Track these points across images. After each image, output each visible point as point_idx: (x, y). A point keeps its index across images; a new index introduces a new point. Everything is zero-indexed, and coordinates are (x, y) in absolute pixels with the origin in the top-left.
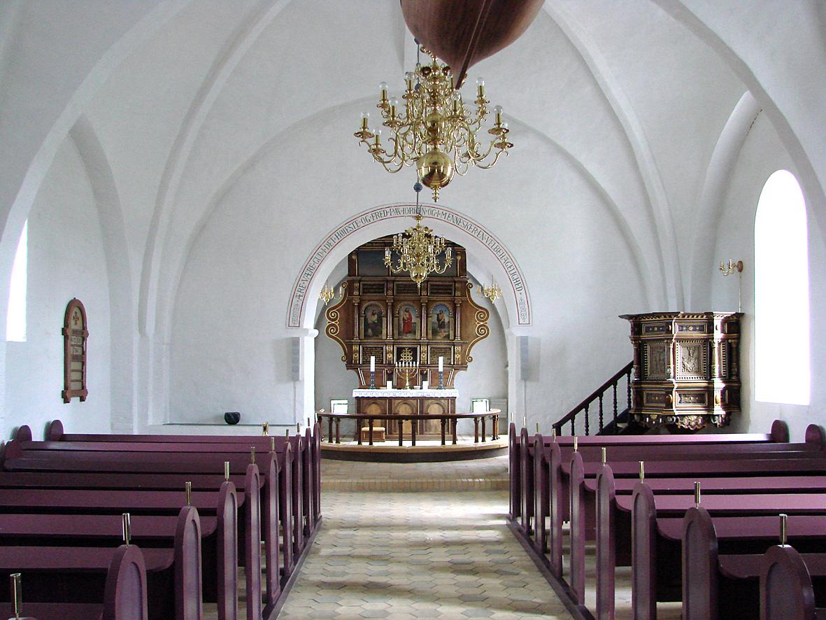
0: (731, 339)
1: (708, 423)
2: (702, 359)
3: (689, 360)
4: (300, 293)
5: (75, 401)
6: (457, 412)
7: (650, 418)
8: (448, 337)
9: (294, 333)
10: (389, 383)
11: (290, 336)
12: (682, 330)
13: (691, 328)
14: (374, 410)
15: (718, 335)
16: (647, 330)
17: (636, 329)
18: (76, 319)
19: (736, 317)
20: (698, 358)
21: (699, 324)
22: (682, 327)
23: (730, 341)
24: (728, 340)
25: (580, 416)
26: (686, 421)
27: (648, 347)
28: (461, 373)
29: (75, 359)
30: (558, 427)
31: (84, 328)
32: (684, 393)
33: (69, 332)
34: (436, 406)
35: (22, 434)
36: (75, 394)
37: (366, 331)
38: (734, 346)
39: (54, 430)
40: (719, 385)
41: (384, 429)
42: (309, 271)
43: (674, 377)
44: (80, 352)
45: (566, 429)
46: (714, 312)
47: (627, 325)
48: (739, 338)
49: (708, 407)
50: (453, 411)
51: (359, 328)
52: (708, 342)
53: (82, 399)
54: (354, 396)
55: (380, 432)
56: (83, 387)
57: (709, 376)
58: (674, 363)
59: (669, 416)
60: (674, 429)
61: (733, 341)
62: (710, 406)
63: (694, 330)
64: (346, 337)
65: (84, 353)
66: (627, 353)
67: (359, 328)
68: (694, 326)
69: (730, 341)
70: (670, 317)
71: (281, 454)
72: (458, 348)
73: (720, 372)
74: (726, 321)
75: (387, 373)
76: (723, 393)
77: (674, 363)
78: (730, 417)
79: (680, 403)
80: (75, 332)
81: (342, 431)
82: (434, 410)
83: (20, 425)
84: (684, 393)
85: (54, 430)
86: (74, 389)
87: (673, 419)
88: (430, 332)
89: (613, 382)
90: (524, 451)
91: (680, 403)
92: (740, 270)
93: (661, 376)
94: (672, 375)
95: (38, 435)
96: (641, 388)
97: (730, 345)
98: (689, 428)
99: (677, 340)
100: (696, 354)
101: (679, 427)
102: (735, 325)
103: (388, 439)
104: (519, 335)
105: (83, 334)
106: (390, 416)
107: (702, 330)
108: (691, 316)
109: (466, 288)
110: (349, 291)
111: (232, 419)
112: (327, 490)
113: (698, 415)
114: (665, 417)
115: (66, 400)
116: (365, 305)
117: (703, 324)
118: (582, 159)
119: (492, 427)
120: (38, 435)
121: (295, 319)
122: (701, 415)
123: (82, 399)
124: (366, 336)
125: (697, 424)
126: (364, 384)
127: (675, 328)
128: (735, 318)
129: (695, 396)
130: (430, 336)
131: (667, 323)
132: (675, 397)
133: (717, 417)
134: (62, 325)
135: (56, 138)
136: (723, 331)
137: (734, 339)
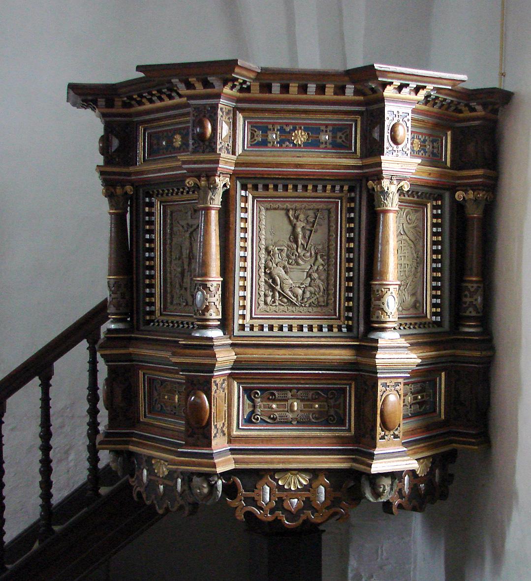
0: (465, 188)
2: (340, 254)
3: (292, 259)
7: (151, 472)
12: (264, 143)
13: (301, 137)
17: (115, 143)
19: (485, 106)
20: (327, 254)
21: (333, 120)
22: (265, 130)
23: (459, 195)
24: (453, 189)
27: (158, 208)
38: (474, 213)
43: (225, 324)
46: (377, 66)
49: (357, 439)
58: (226, 269)
59: (200, 474)
61: (471, 195)
63: (313, 143)
68: (313, 130)
69: (459, 195)
70: (207, 84)
73: (121, 347)
77: (226, 269)
78: (451, 469)
79: (249, 421)
87: (213, 487)
91: (249, 421)
94: (215, 314)
96: (129, 358)
97: (459, 209)
98: (277, 521)
100: (319, 237)
101: (240, 516)
107: (341, 145)
108: (312, 87)
113: (314, 473)
117: (345, 120)
119: (86, 375)
122: (329, 473)
125: (308, 504)
128: (480, 111)
129: (309, 395)
131: (197, 108)
133: (386, 482)
137: (474, 187)
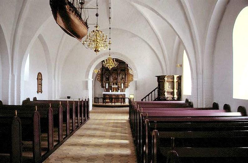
1: (173, 99)
4: (88, 71)
5: (40, 93)
6: (126, 97)
8: (124, 81)
9: (87, 80)
10: (110, 91)
11: (86, 80)
14: (107, 97)
15: (176, 80)
16: (161, 79)
18: (40, 76)
25: (147, 97)
26: (168, 98)
28: (127, 89)
29: (40, 84)
30: (142, 100)
31: (42, 78)
32: (168, 92)
33: (38, 79)
34: (121, 96)
35: (28, 99)
36: (40, 92)
37: (106, 79)
39: (35, 99)
40: (176, 91)
41: (109, 101)
42: (90, 67)
44: (41, 78)
45: (144, 100)
47: (157, 78)
48: (181, 81)
50: (125, 97)
51: (104, 79)
52: (173, 82)
53: (41, 93)
54: (103, 93)
55: (108, 102)
56: (42, 90)
57: (173, 89)
60: (165, 100)
62: (174, 95)
64: (102, 81)
65: (42, 83)
66: (156, 85)
67: (104, 79)
71: (81, 106)
72: (126, 83)
74: (178, 77)
75: (110, 88)
76: (177, 92)
80: (40, 79)
81: (99, 101)
82: (121, 97)
83: (28, 98)
84: (168, 92)
85: (35, 99)
86: (40, 91)
88: (120, 79)
89: (154, 90)
90: (131, 106)
92: (181, 66)
93: (163, 89)
95: (31, 100)
99: (167, 81)
102: (180, 78)
103: (110, 103)
104: (135, 80)
105: (41, 79)
106: (111, 98)
107: (172, 79)
109: (128, 70)
110: (102, 71)
111: (69, 98)
112: (90, 113)
114: (164, 98)
115: (38, 93)
116: (106, 74)
118: (148, 42)
120: (31, 100)
121: (87, 75)
123: (41, 93)
124: (106, 80)
126: (105, 91)
127: (166, 79)
130: (120, 80)
132: (166, 94)
134: (37, 78)
135: (36, 36)
136: (177, 79)
